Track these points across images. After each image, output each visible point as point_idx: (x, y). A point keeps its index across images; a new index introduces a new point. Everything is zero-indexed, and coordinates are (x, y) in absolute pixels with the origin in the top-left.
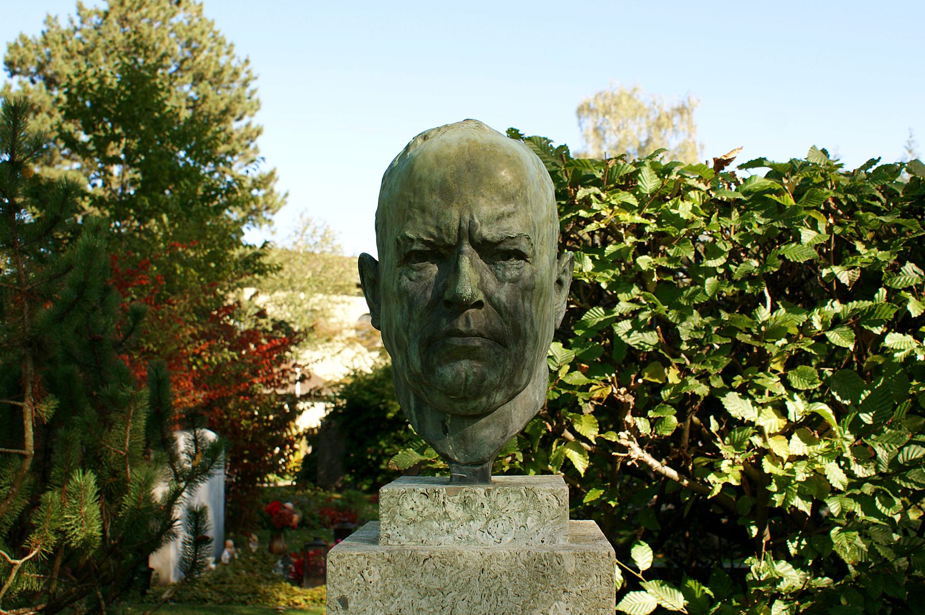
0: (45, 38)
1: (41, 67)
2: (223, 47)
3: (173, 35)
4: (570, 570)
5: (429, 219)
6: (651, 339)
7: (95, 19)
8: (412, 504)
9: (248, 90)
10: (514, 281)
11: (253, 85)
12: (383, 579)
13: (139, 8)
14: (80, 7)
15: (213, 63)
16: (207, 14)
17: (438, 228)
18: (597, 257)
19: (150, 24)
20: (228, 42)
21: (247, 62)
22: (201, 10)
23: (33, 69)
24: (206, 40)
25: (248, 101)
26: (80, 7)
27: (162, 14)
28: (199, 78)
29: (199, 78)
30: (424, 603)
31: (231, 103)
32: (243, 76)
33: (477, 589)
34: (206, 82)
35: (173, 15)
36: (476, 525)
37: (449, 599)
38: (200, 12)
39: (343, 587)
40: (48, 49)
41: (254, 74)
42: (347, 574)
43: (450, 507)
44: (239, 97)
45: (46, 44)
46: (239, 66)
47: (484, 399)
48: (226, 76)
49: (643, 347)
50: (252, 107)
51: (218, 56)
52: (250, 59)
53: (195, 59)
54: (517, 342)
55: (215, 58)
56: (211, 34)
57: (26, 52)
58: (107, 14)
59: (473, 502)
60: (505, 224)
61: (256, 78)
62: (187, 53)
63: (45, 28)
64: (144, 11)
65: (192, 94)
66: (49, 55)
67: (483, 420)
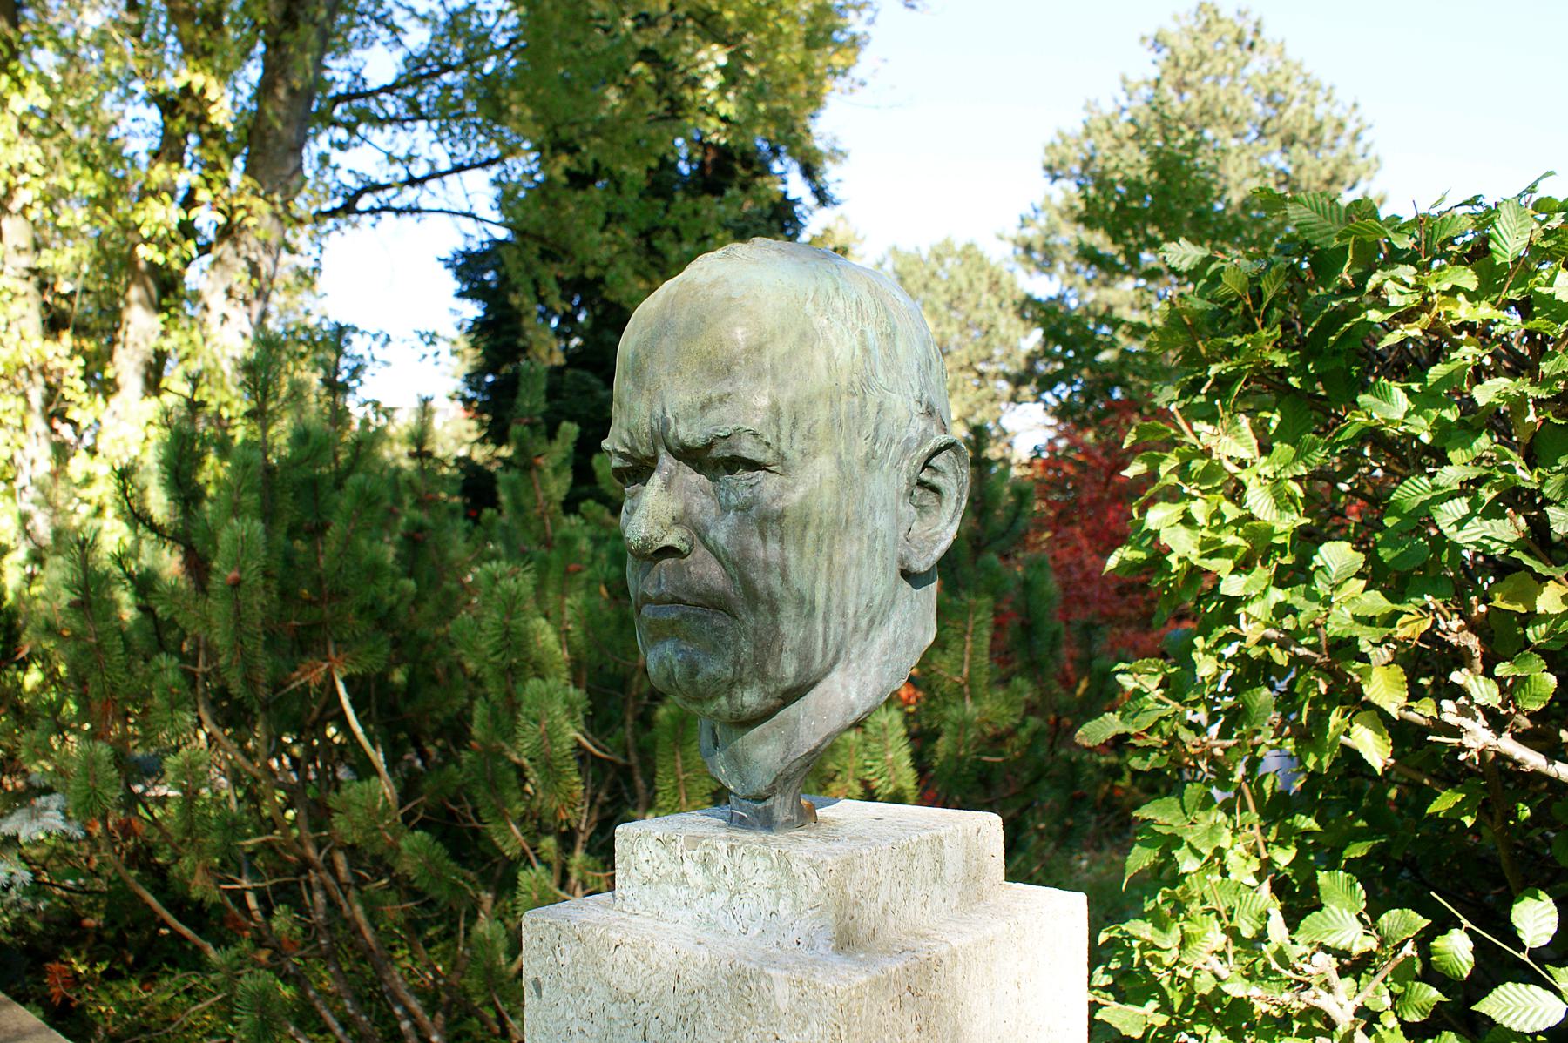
0: (1087, 127)
1: (1085, 165)
2: (1319, 93)
3: (1249, 91)
6: (1506, 531)
7: (1146, 92)
8: (647, 856)
9: (1360, 145)
10: (745, 508)
11: (1366, 137)
13: (1200, 65)
14: (1124, 81)
15: (1306, 118)
16: (1292, 54)
18: (1415, 387)
19: (1216, 82)
20: (1326, 85)
21: (1355, 106)
22: (1283, 50)
23: (1077, 169)
24: (1293, 88)
25: (1362, 160)
26: (1124, 81)
27: (1231, 66)
28: (1289, 141)
29: (1289, 141)
30: (614, 1011)
31: (1337, 167)
32: (1351, 127)
33: (670, 1004)
34: (1298, 146)
35: (1246, 63)
36: (720, 899)
38: (1282, 51)
40: (1092, 141)
41: (1367, 121)
44: (1348, 157)
45: (1088, 135)
46: (1344, 115)
47: (723, 700)
48: (1327, 135)
49: (1488, 546)
50: (1369, 168)
51: (1312, 106)
52: (1360, 101)
53: (1281, 116)
54: (754, 610)
55: (1309, 111)
56: (1301, 79)
57: (1066, 150)
58: (1158, 81)
60: (713, 416)
61: (1370, 126)
62: (1270, 111)
63: (1085, 116)
64: (1206, 67)
65: (1282, 164)
66: (1094, 148)
67: (756, 730)
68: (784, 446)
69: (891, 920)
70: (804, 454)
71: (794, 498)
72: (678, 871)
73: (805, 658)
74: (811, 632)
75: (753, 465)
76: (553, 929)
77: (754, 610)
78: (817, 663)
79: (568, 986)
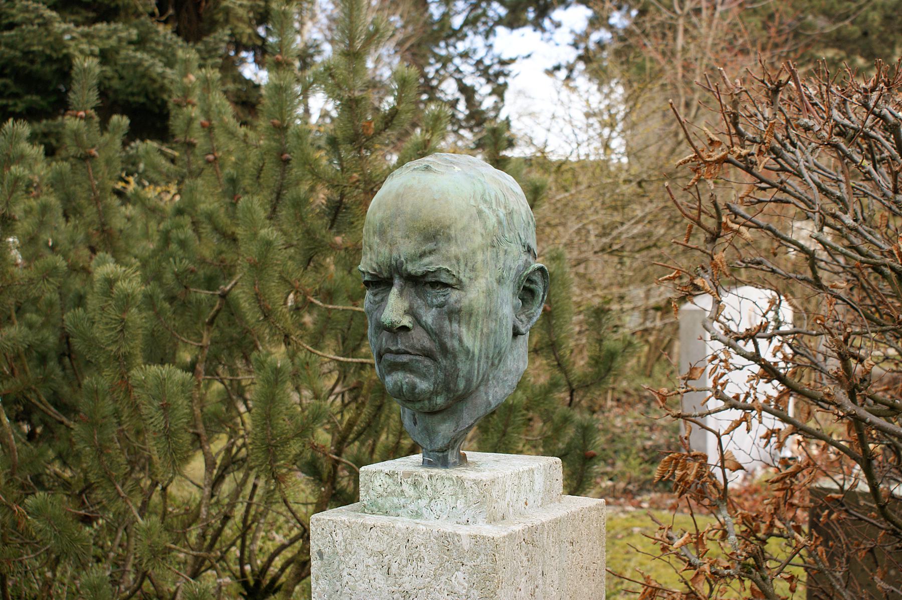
4: (466, 548)
10: (440, 306)
36: (423, 503)
37: (386, 560)
39: (320, 543)
43: (405, 487)
60: (426, 260)
68: (461, 276)
69: (511, 510)
70: (471, 279)
71: (465, 302)
72: (399, 490)
73: (469, 381)
74: (472, 367)
75: (446, 285)
77: (445, 357)
78: (474, 384)
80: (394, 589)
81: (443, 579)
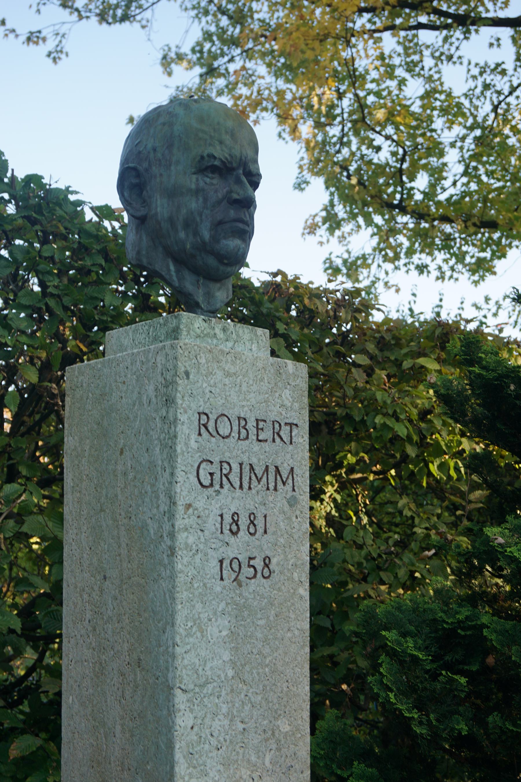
5: (224, 149)
8: (198, 325)
12: (207, 363)
17: (230, 155)
30: (227, 381)
39: (187, 365)
42: (189, 356)
43: (217, 331)
59: (228, 329)
72: (212, 332)
76: (196, 347)
79: (204, 372)
80: (244, 403)
81: (277, 395)
